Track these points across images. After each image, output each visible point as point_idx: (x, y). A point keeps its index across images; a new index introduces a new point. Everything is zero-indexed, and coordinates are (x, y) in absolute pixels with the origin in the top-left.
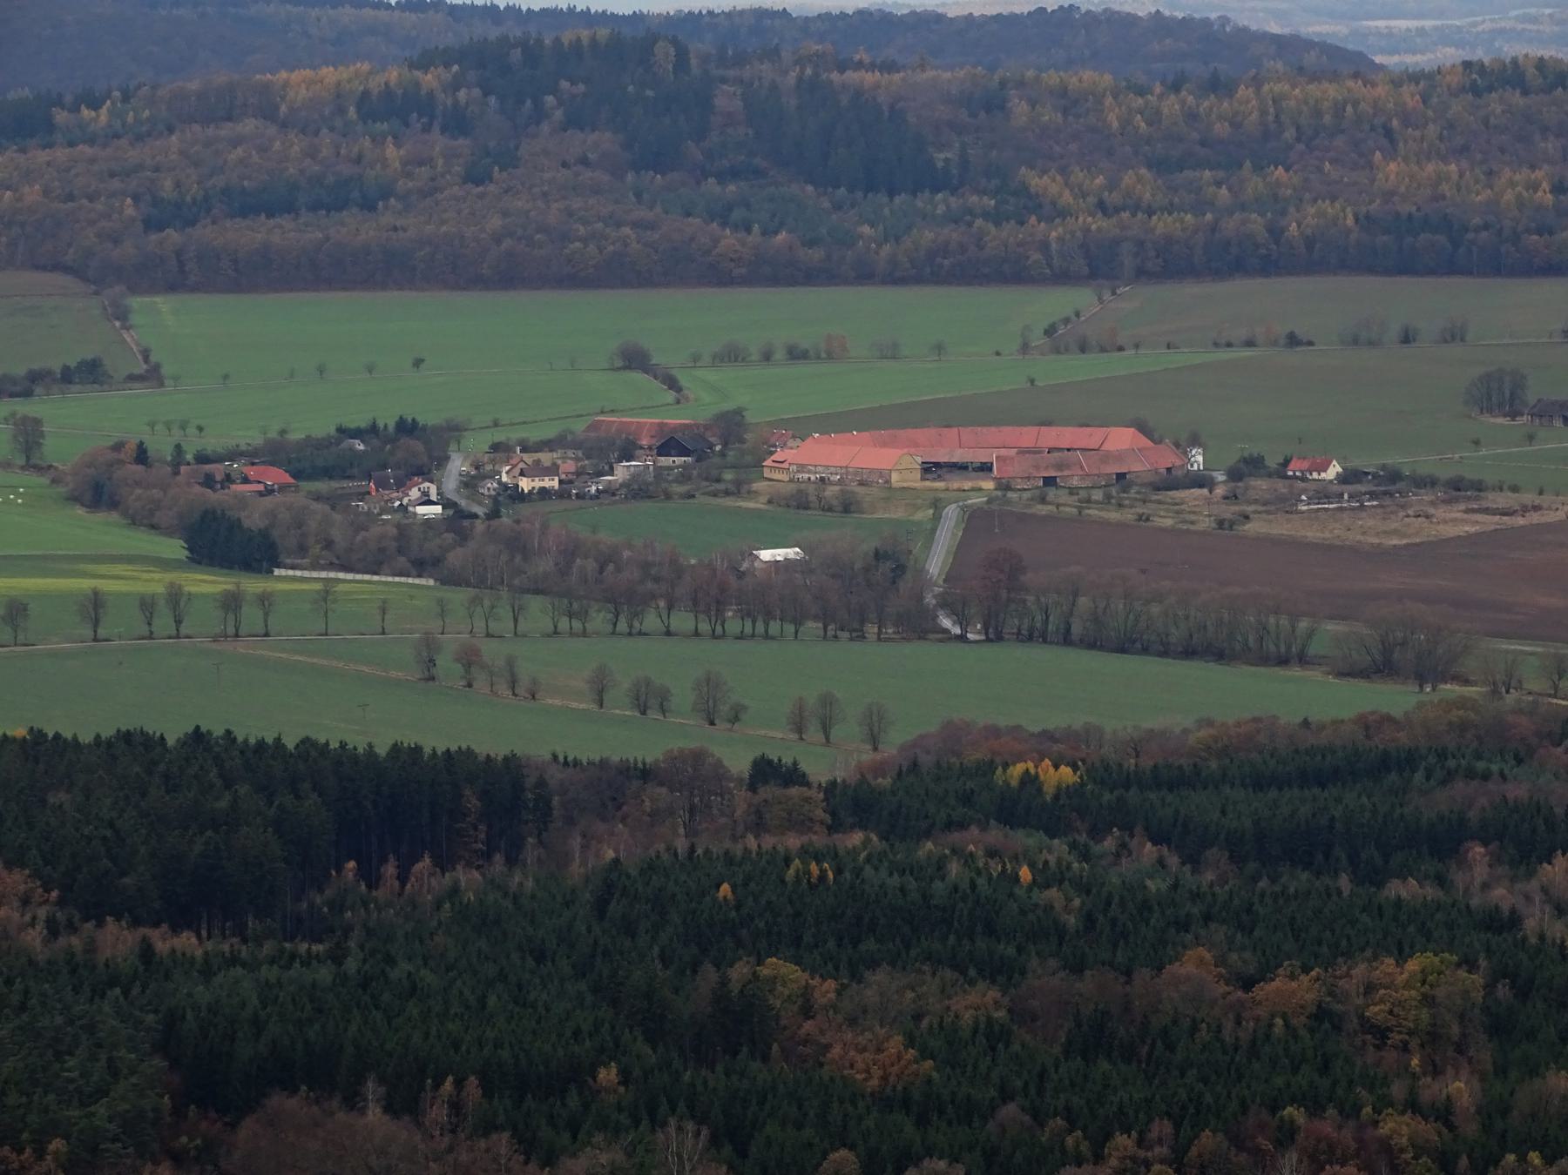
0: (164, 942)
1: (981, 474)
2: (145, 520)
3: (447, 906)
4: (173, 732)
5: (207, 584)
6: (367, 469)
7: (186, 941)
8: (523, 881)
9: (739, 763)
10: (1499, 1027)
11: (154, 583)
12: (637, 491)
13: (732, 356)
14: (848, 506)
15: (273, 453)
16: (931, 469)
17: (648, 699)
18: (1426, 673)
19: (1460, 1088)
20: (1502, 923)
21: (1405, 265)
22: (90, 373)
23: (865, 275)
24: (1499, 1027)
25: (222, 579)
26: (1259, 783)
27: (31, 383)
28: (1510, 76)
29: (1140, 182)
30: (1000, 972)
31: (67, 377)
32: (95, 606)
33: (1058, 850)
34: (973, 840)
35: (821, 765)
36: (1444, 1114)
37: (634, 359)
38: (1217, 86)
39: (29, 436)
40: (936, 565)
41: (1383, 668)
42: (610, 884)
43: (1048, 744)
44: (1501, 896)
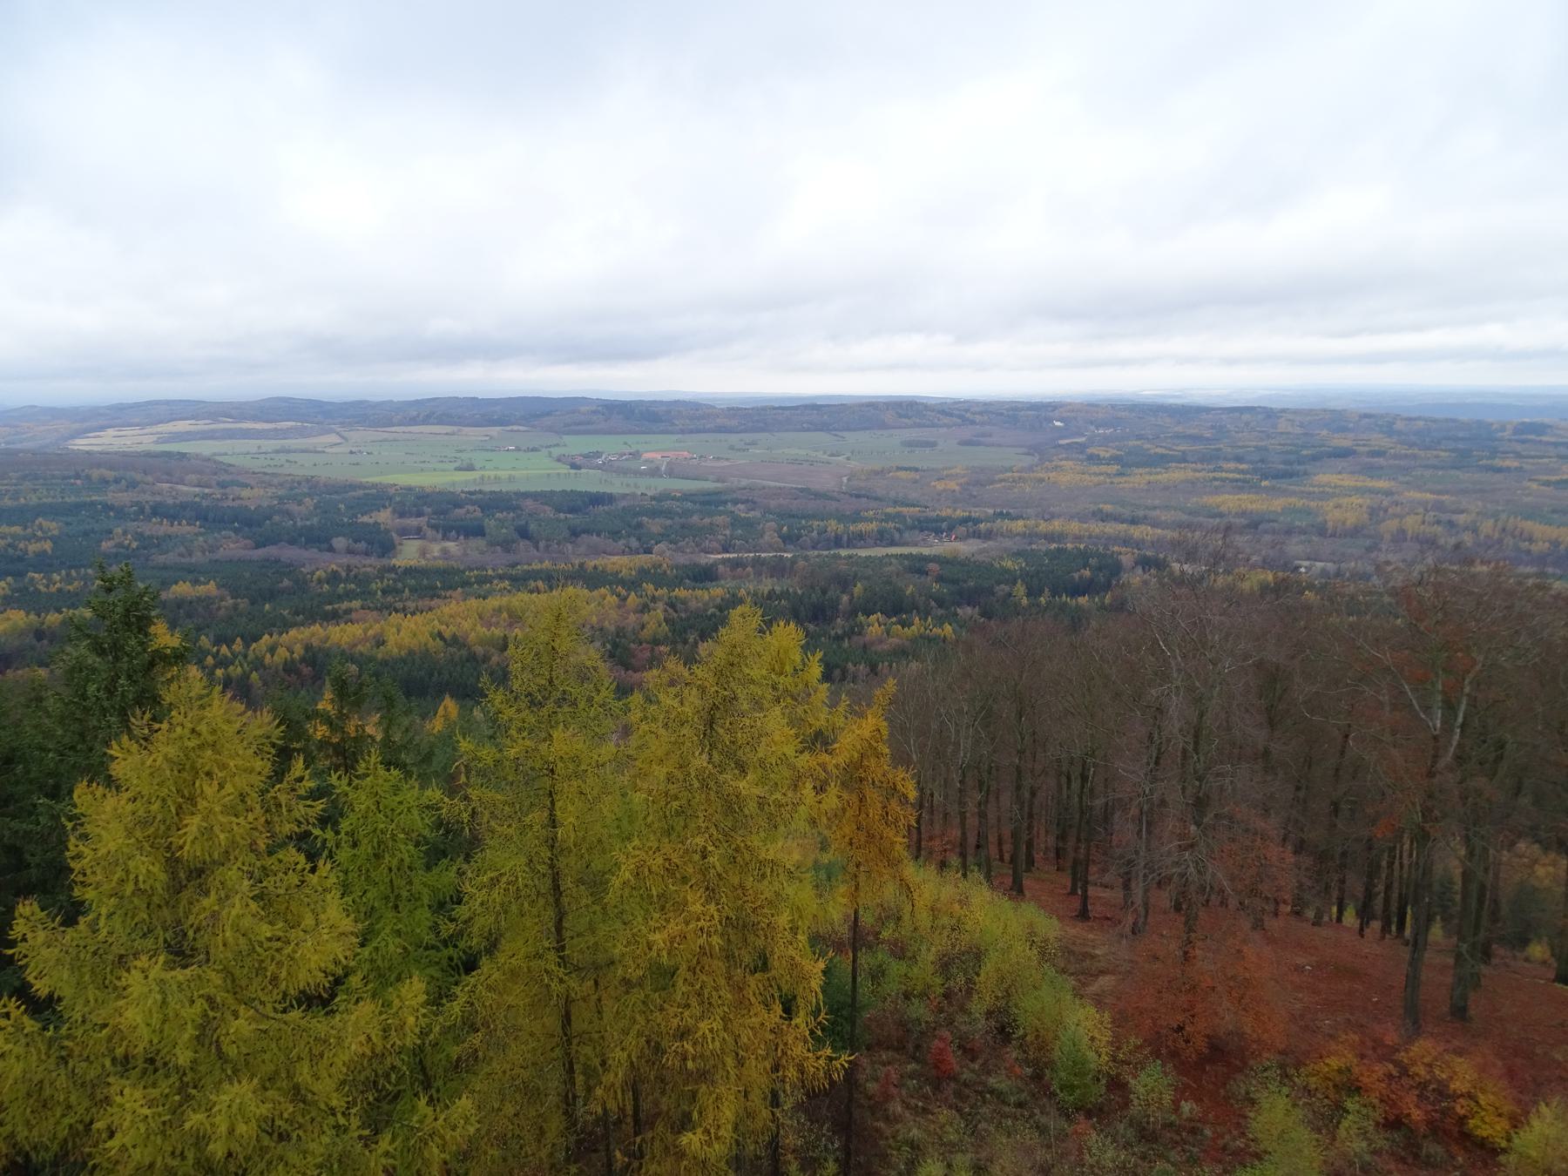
0: (568, 516)
1: (1413, 415)
2: (564, 463)
3: (1016, 678)
4: (569, 490)
5: (573, 471)
6: (593, 457)
7: (571, 516)
8: (613, 508)
9: (639, 493)
10: (732, 524)
11: (566, 471)
12: (626, 460)
13: (638, 443)
14: (652, 462)
15: (580, 455)
16: (910, 444)
17: (628, 485)
18: (723, 482)
19: (728, 532)
20: (732, 512)
21: (720, 432)
22: (558, 445)
23: (654, 433)
24: (732, 524)
25: (81, 448)
26: (704, 495)
27: (550, 447)
28: (733, 409)
29: (687, 421)
30: (672, 519)
31: (555, 446)
32: (558, 474)
33: (678, 504)
34: (668, 502)
35: (650, 494)
36: (725, 535)
37: (625, 443)
38: (697, 410)
39: (550, 453)
40: (663, 469)
41: (718, 481)
42: (624, 508)
43: (677, 491)
44: (733, 509)
